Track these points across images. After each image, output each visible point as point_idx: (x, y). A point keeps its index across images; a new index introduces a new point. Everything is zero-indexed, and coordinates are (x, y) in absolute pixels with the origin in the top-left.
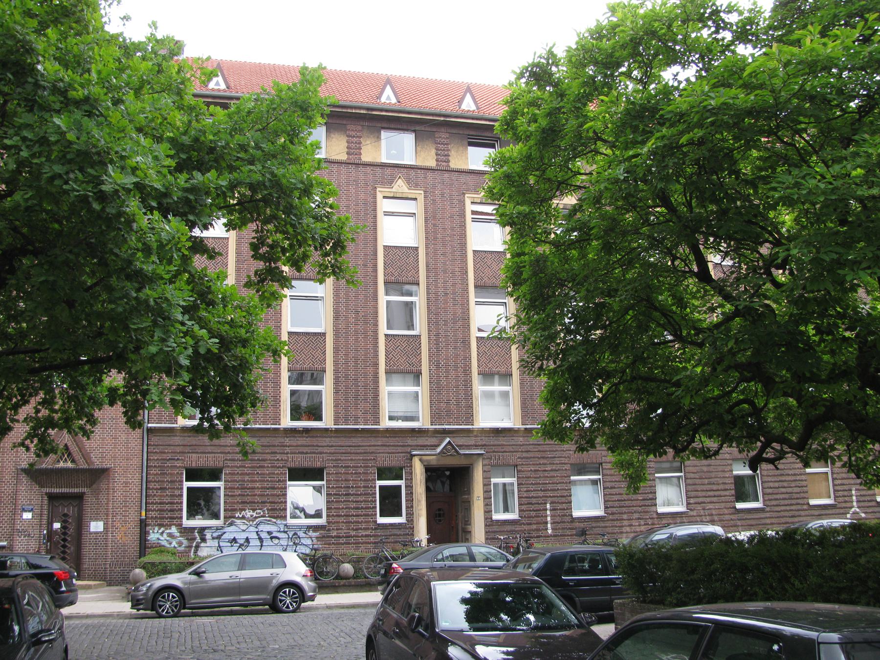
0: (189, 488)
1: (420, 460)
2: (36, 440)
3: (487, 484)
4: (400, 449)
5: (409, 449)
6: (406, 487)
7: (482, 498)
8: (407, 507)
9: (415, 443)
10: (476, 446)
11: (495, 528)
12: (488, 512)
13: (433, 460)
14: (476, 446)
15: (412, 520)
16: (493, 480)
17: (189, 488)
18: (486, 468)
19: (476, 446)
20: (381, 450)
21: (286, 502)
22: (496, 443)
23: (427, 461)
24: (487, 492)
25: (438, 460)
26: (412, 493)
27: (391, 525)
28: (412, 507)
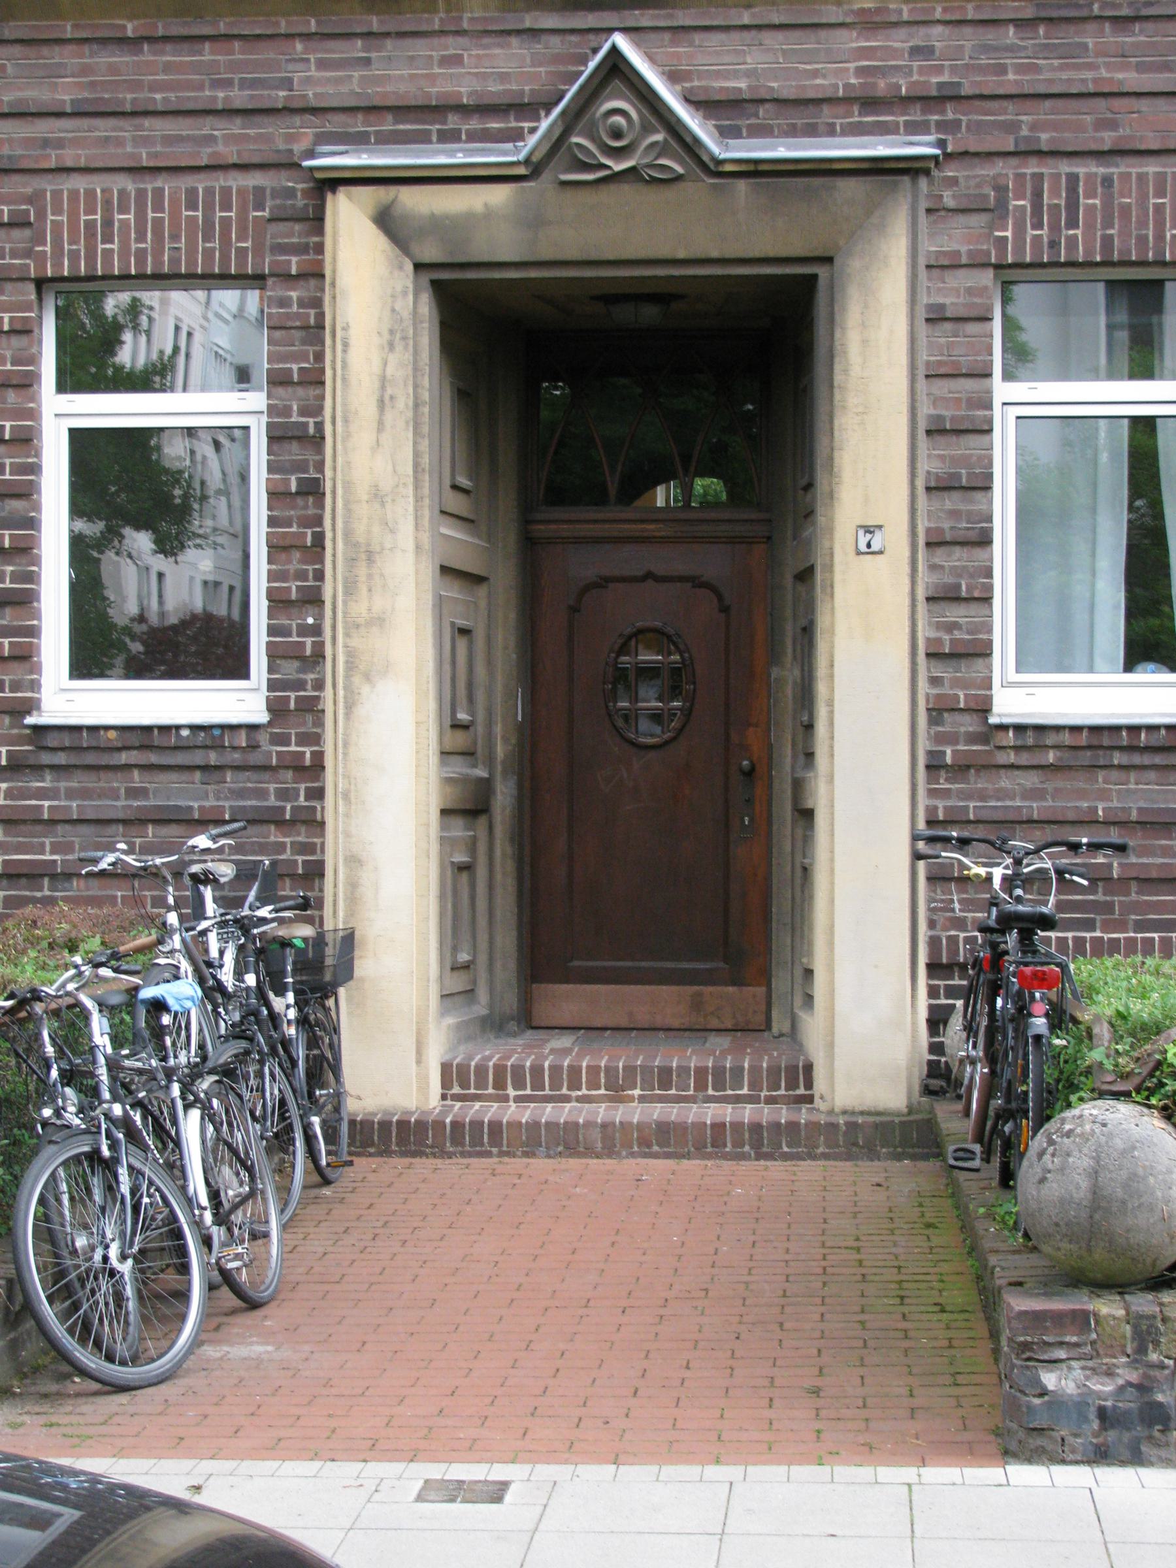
0: (81, 440)
1: (385, 220)
2: (130, 1262)
3: (952, 431)
4: (225, 139)
5: (277, 136)
6: (276, 437)
7: (896, 538)
8: (278, 602)
9: (349, 85)
10: (870, 103)
11: (1013, 793)
12: (953, 655)
13: (487, 218)
14: (870, 103)
15: (311, 707)
16: (1014, 398)
17: (81, 440)
18: (953, 291)
19: (870, 105)
20: (81, 141)
21: (272, 685)
22: (1053, 74)
23: (438, 225)
24: (953, 490)
25: (532, 221)
26: (313, 490)
27: (143, 737)
28: (313, 599)
